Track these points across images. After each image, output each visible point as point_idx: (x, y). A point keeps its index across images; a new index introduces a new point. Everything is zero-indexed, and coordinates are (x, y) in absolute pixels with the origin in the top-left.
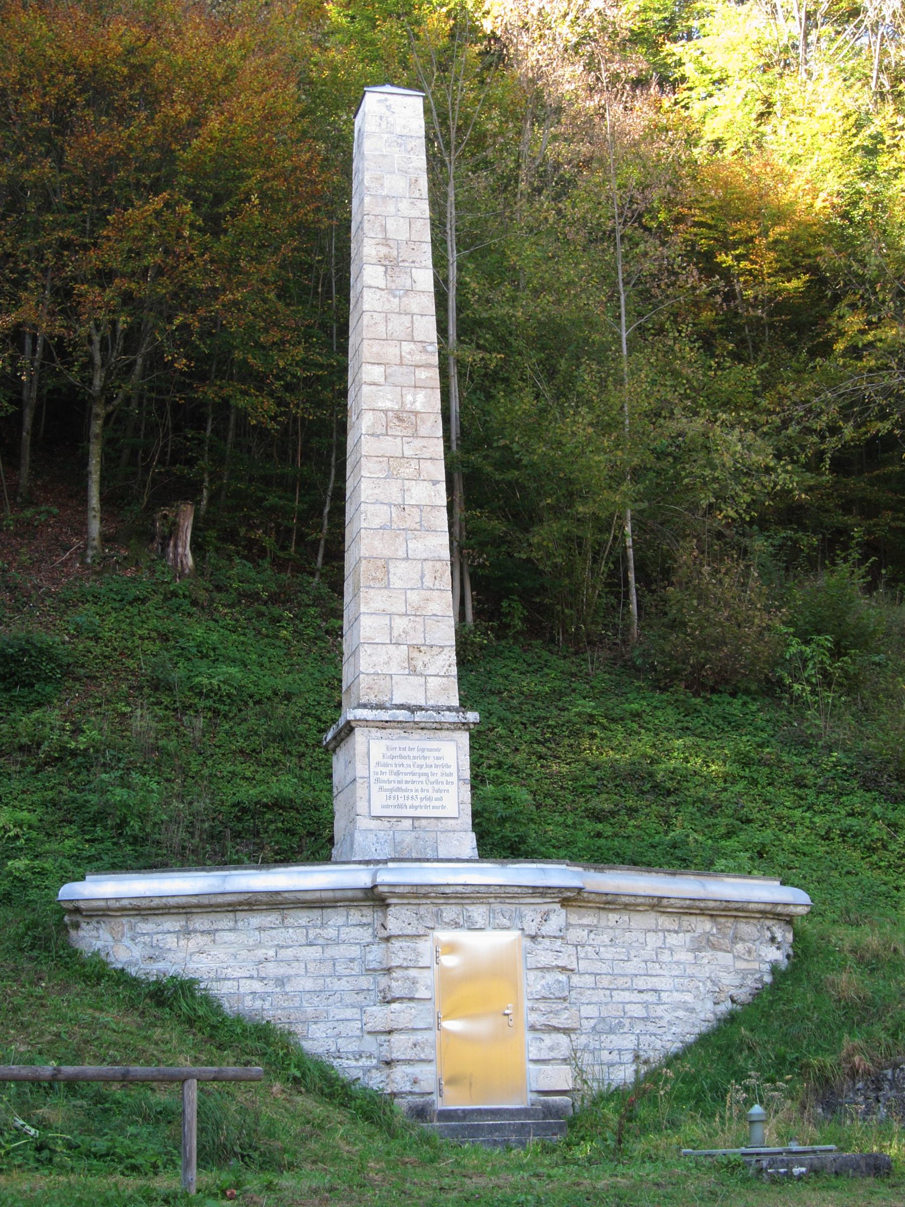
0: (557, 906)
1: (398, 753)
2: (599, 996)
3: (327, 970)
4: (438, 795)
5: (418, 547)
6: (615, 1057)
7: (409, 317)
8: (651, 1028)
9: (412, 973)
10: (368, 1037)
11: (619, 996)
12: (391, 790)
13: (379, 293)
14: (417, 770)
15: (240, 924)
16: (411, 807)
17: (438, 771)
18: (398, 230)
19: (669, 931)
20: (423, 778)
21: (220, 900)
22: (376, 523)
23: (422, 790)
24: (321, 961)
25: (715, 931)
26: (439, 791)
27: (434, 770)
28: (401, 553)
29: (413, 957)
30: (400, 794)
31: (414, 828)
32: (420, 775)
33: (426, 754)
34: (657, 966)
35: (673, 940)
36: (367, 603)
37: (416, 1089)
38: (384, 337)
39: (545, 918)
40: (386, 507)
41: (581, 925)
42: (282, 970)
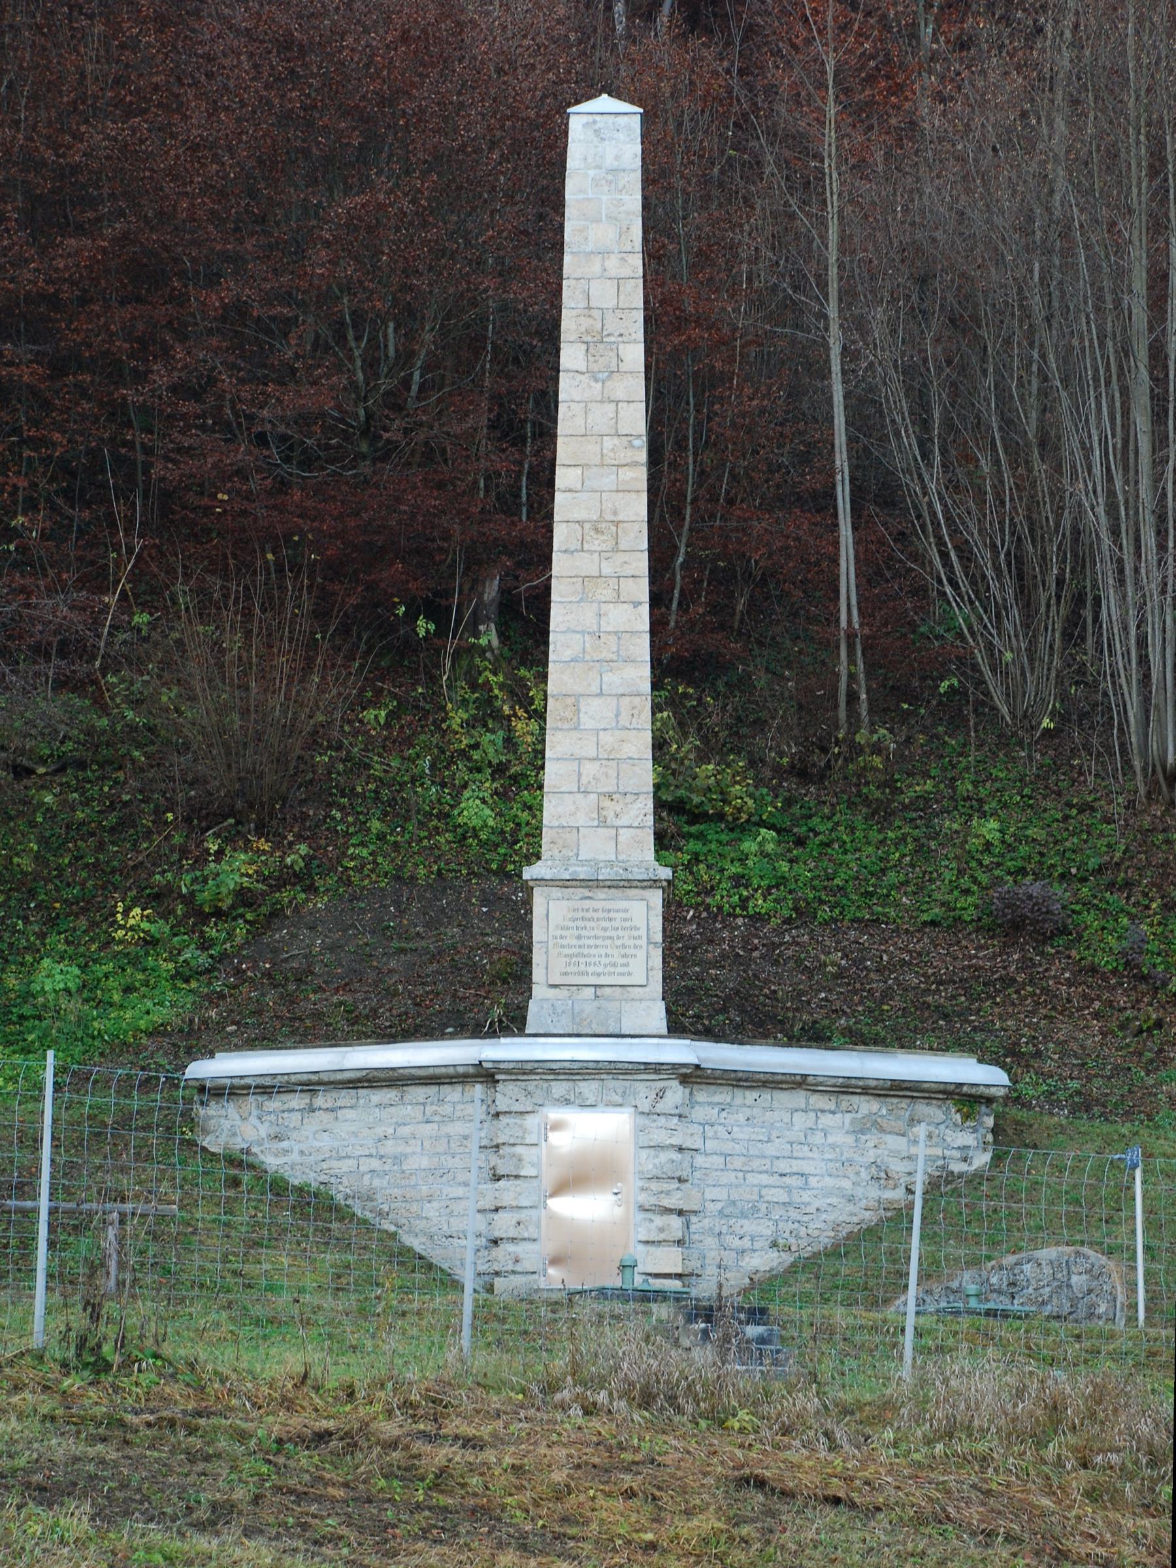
0: (675, 1084)
1: (580, 914)
2: (730, 1177)
3: (442, 1147)
4: (624, 961)
5: (613, 680)
6: (746, 1243)
7: (613, 405)
8: (794, 1214)
9: (519, 1150)
10: (479, 1216)
11: (752, 1179)
12: (571, 956)
13: (579, 377)
14: (601, 933)
15: (362, 1101)
16: (594, 974)
17: (626, 934)
18: (603, 293)
19: (823, 1111)
20: (608, 942)
21: (339, 1076)
22: (567, 654)
23: (607, 955)
24: (437, 1138)
25: (884, 1112)
26: (625, 956)
27: (621, 933)
28: (595, 689)
29: (520, 1134)
30: (582, 960)
31: (597, 997)
32: (604, 938)
33: (612, 915)
34: (806, 1148)
35: (826, 1120)
36: (552, 748)
37: (518, 1268)
38: (583, 431)
39: (661, 1094)
40: (579, 636)
41: (709, 1104)
42: (401, 1148)
